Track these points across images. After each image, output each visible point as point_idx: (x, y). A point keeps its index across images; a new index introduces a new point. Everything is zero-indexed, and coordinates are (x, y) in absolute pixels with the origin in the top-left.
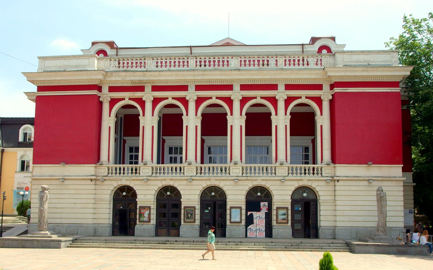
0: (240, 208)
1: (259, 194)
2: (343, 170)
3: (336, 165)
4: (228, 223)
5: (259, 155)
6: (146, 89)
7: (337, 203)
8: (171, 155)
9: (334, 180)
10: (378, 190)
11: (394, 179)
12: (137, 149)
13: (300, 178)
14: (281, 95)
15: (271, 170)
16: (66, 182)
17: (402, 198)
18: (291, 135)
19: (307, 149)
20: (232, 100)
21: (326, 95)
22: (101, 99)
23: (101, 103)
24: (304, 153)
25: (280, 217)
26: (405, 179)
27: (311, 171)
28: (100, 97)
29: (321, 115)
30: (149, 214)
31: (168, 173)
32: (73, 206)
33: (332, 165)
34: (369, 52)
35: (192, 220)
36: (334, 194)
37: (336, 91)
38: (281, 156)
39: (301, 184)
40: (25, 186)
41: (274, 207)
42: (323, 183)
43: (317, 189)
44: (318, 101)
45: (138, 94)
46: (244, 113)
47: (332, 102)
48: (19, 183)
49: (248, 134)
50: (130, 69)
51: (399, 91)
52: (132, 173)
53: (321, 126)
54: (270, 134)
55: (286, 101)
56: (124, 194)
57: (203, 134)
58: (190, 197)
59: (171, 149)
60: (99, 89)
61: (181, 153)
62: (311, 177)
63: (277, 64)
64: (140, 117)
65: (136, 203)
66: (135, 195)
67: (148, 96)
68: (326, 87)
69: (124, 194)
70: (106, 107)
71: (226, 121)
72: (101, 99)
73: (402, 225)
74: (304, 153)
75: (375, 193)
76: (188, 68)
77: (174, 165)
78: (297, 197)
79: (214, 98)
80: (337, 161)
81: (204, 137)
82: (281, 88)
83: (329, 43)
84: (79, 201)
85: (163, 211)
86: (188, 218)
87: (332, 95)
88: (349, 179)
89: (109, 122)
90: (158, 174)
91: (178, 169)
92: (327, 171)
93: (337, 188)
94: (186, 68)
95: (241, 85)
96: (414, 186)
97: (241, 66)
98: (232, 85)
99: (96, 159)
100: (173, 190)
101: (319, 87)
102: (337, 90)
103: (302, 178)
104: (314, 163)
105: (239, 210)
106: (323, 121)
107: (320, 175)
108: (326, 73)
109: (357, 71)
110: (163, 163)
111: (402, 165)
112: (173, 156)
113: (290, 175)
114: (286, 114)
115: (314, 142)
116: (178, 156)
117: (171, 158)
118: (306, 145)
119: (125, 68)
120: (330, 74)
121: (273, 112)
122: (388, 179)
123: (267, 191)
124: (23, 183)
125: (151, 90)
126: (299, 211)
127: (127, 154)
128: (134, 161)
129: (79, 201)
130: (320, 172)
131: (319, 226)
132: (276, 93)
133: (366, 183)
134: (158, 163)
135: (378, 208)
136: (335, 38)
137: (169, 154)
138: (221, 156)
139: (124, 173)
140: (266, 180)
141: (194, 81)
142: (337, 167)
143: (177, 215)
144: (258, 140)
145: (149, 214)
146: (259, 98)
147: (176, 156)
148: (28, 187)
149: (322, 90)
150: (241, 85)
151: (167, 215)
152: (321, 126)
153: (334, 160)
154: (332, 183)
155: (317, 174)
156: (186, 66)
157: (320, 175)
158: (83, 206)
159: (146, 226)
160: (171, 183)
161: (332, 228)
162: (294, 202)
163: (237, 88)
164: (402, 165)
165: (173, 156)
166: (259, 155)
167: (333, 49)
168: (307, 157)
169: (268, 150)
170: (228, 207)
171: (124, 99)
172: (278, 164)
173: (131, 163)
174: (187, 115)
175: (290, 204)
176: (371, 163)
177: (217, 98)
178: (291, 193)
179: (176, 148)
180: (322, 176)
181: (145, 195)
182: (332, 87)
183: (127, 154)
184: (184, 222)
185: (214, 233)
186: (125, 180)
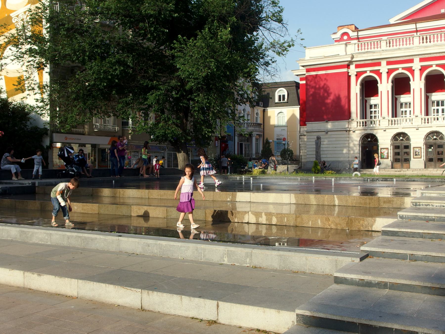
16: (329, 133)
22: (350, 74)
23: (349, 77)
30: (388, 153)
35: (420, 157)
40: (282, 137)
48: (278, 135)
50: (369, 50)
55: (356, 75)
56: (369, 139)
66: (408, 139)
69: (369, 139)
70: (353, 79)
72: (350, 74)
76: (413, 46)
85: (397, 151)
86: (416, 155)
89: (356, 89)
94: (379, 49)
100: (404, 135)
110: (396, 117)
116: (408, 110)
119: (366, 50)
124: (281, 135)
134: (393, 117)
135: (316, 146)
139: (428, 123)
143: (408, 154)
145: (388, 153)
146: (400, 69)
148: (285, 138)
151: (401, 154)
156: (411, 44)
160: (403, 131)
184: (414, 158)
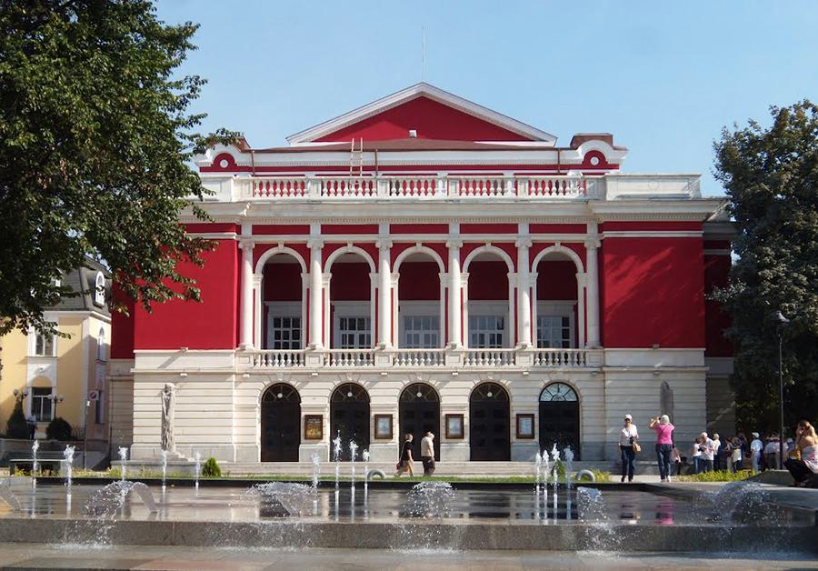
0: (532, 416)
1: (490, 394)
2: (616, 356)
3: (606, 349)
4: (513, 438)
5: (422, 334)
6: (312, 231)
8: (344, 332)
9: (601, 371)
10: (662, 387)
11: (692, 369)
12: (297, 322)
13: (552, 369)
14: (523, 240)
15: (573, 358)
17: (136, 400)
19: (565, 321)
20: (448, 249)
21: (591, 240)
26: (708, 368)
27: (563, 359)
28: (238, 242)
29: (585, 271)
33: (601, 349)
36: (602, 393)
37: (606, 236)
38: (456, 339)
42: (587, 376)
44: (580, 249)
45: (299, 239)
46: (261, 263)
47: (600, 252)
51: (700, 236)
52: (293, 362)
53: (585, 289)
54: (507, 298)
59: (342, 320)
60: (238, 229)
61: (438, 328)
62: (563, 367)
64: (509, 275)
65: (299, 410)
67: (384, 240)
68: (592, 230)
70: (248, 256)
71: (576, 281)
72: (240, 246)
75: (658, 391)
77: (282, 351)
79: (558, 245)
80: (605, 344)
82: (315, 230)
83: (231, 150)
87: (602, 241)
88: (620, 369)
89: (252, 282)
90: (404, 364)
92: (593, 358)
95: (253, 226)
97: (530, 194)
98: (448, 225)
101: (581, 229)
102: (608, 234)
103: (555, 370)
106: (587, 280)
111: (705, 349)
112: (413, 332)
114: (530, 270)
117: (344, 336)
121: (511, 267)
122: (619, 369)
123: (489, 385)
125: (459, 231)
127: (285, 332)
128: (282, 341)
130: (582, 360)
131: (581, 441)
132: (514, 238)
133: (649, 376)
136: (612, 136)
137: (490, 334)
138: (362, 332)
140: (569, 372)
141: (388, 218)
142: (607, 353)
144: (420, 307)
146: (488, 245)
147: (352, 332)
149: (586, 232)
150: (253, 226)
152: (585, 289)
157: (582, 364)
161: (601, 445)
163: (454, 229)
164: (705, 349)
166: (422, 334)
167: (610, 158)
168: (565, 334)
169: (434, 323)
170: (513, 414)
171: (346, 245)
173: (277, 346)
174: (516, 271)
175: (537, 408)
176: (658, 345)
177: (286, 245)
179: (362, 321)
180: (585, 366)
182: (602, 228)
183: (285, 332)
185: (75, 456)
186: (561, 374)
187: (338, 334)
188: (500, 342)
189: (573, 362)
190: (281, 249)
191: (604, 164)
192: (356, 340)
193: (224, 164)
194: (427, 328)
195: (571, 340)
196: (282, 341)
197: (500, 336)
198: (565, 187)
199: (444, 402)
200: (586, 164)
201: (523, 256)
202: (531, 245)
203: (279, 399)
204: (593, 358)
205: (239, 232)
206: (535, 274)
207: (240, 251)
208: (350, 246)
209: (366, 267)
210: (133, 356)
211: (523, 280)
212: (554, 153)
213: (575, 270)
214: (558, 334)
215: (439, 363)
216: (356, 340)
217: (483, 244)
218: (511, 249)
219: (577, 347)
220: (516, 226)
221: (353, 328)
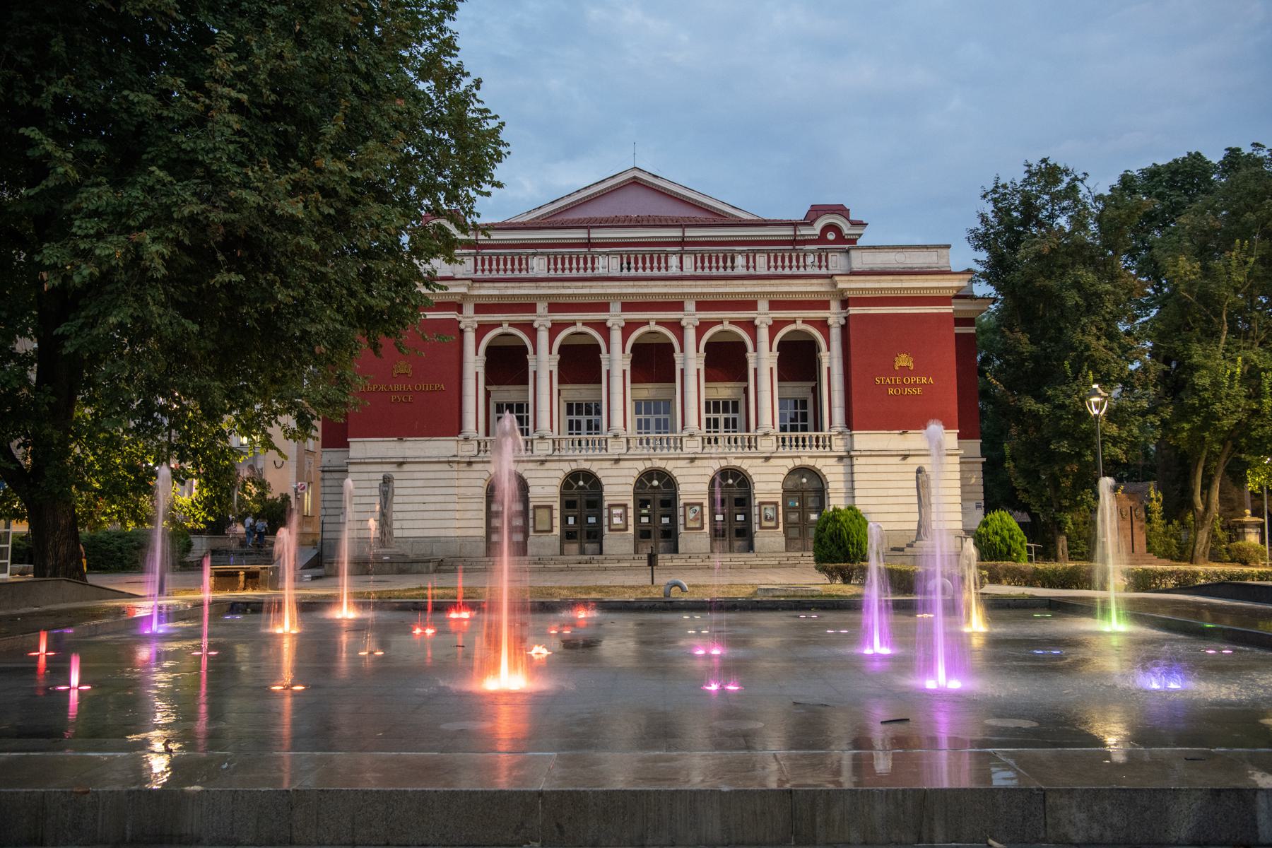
2: (864, 440)
5: (657, 418)
6: (759, 307)
7: (857, 493)
8: (571, 417)
15: (675, 443)
18: (632, 382)
21: (834, 316)
24: (799, 411)
25: (616, 520)
27: (800, 443)
31: (811, 446)
32: (422, 507)
34: (874, 247)
35: (698, 525)
38: (766, 419)
39: (798, 462)
41: (531, 505)
43: (824, 471)
44: (823, 326)
47: (845, 329)
49: (562, 381)
55: (476, 331)
57: (487, 383)
58: (618, 486)
61: (599, 412)
63: (681, 268)
70: (470, 338)
71: (674, 361)
72: (462, 326)
73: (959, 526)
74: (799, 411)
78: (790, 485)
81: (489, 388)
84: (433, 499)
89: (474, 364)
91: (584, 443)
93: (856, 469)
96: (983, 463)
99: (454, 427)
100: (589, 477)
102: (853, 310)
104: (816, 430)
105: (546, 512)
106: (830, 359)
107: (828, 449)
108: (835, 285)
109: (595, 287)
112: (575, 417)
113: (781, 449)
115: (816, 391)
117: (571, 422)
118: (802, 396)
120: (840, 286)
121: (677, 348)
126: (795, 508)
127: (584, 417)
129: (433, 499)
147: (579, 418)
153: (849, 424)
154: (847, 461)
155: (824, 447)
157: (828, 449)
158: (438, 507)
159: (545, 538)
160: (585, 466)
162: (787, 493)
165: (575, 417)
166: (657, 418)
167: (847, 230)
169: (668, 405)
172: (686, 433)
178: (781, 478)
181: (543, 486)
187: (565, 419)
188: (666, 427)
189: (811, 446)
190: (506, 329)
191: (840, 238)
192: (584, 425)
193: (831, 236)
194: (589, 412)
195: (810, 422)
196: (799, 423)
197: (666, 420)
198: (593, 263)
199: (607, 490)
200: (822, 239)
201: (764, 334)
202: (623, 324)
203: (652, 487)
204: (839, 445)
205: (460, 312)
206: (776, 354)
207: (462, 331)
208: (505, 325)
209: (742, 346)
210: (347, 445)
211: (764, 359)
212: (792, 228)
213: (745, 349)
214: (802, 418)
215: (676, 448)
216: (584, 425)
217: (500, 325)
218: (603, 328)
219: (748, 430)
220: (756, 302)
221: (579, 413)
